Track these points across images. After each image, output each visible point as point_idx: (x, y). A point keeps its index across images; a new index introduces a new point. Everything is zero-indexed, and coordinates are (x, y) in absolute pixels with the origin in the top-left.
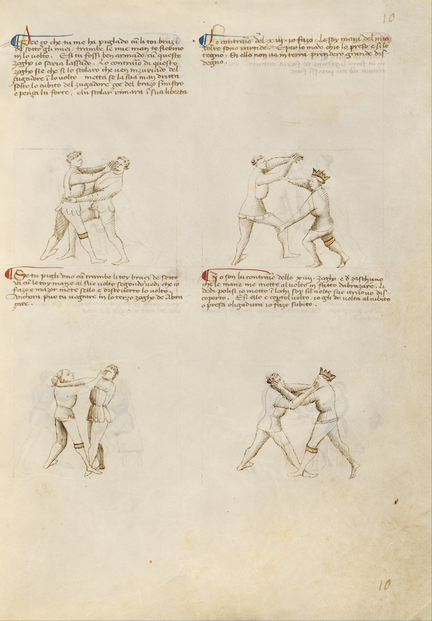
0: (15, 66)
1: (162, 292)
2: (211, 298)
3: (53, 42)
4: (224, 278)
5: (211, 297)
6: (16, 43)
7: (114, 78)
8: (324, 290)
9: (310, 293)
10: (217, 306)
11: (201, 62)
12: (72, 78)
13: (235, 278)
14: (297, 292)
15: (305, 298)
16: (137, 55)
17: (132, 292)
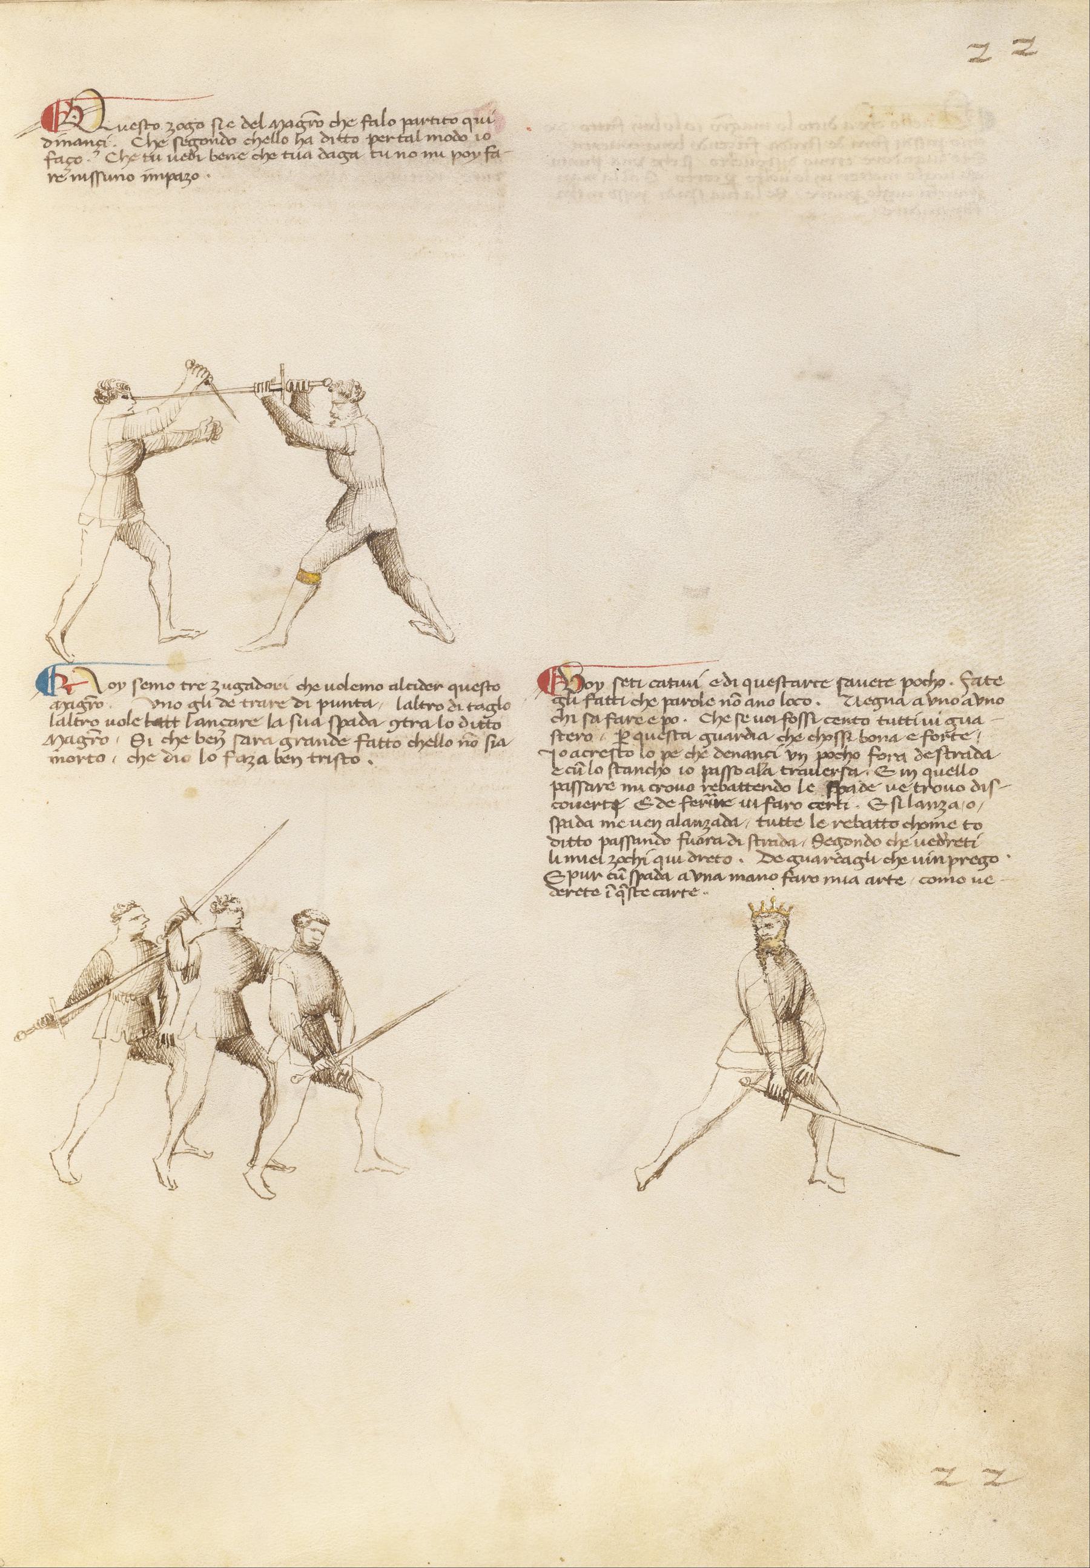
0: (614, 865)
6: (50, 685)
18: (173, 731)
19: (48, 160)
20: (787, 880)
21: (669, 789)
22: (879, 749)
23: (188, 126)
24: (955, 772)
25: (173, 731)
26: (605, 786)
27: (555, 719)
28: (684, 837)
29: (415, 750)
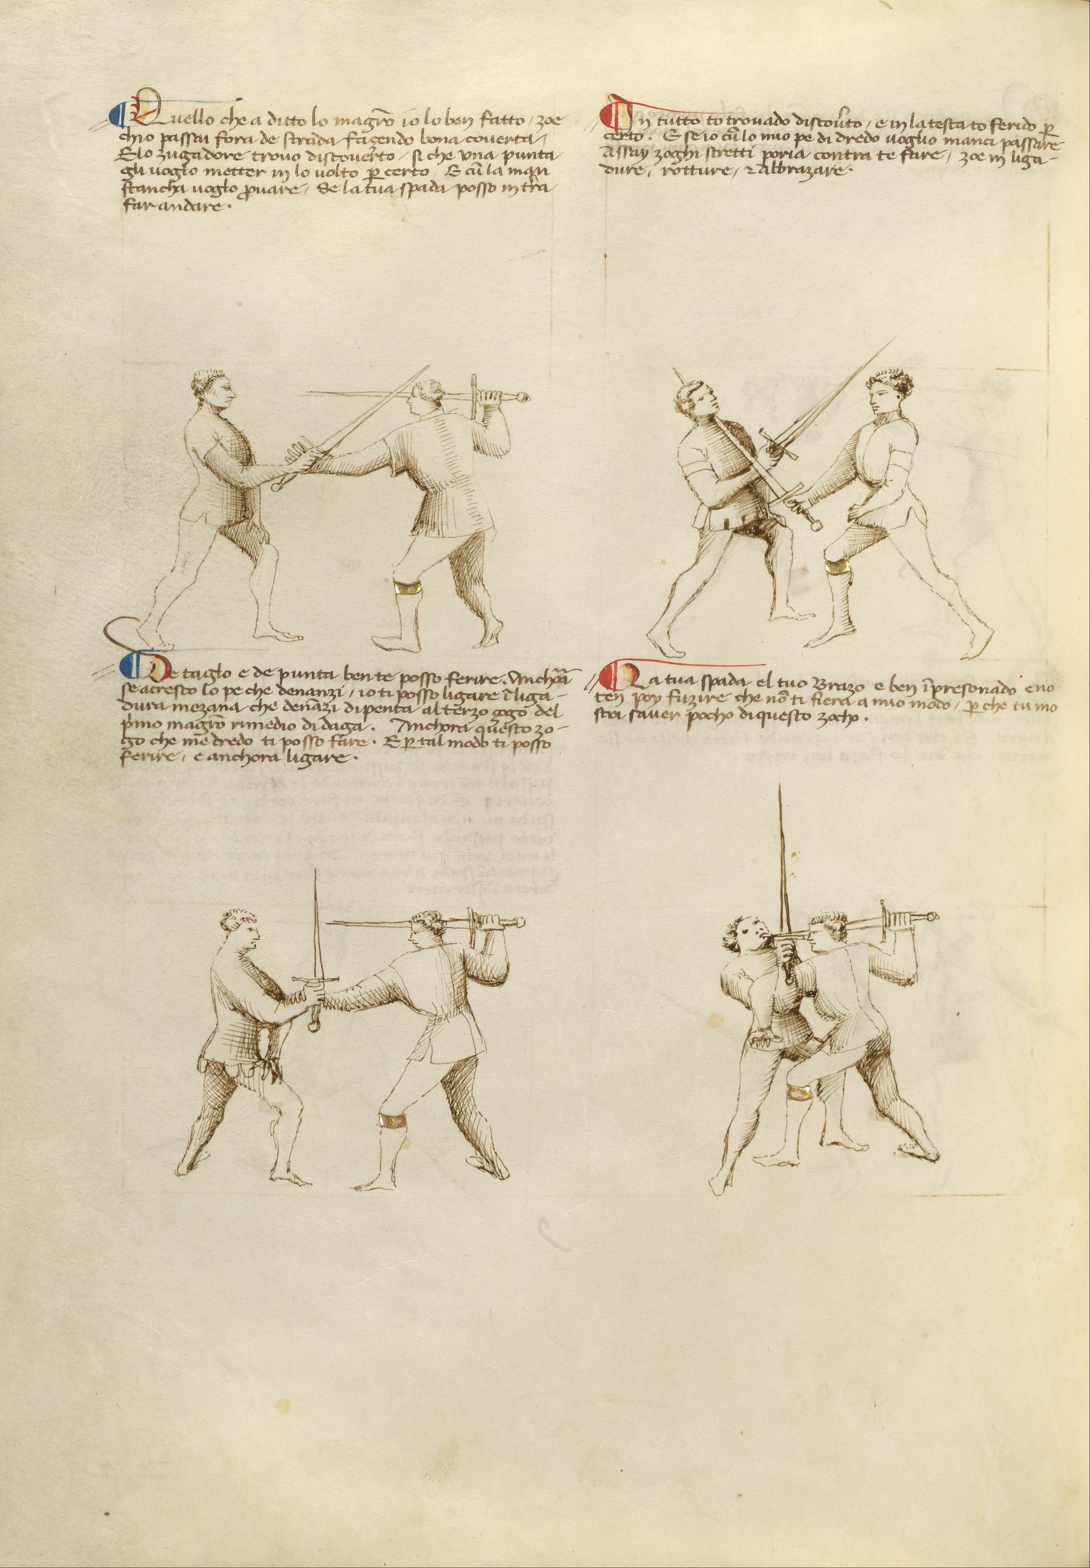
2: (370, 710)
3: (542, 678)
5: (770, 152)
7: (698, 137)
8: (325, 164)
10: (170, 693)
14: (437, 680)
16: (729, 679)
18: (921, 131)
21: (275, 157)
22: (679, 692)
23: (675, 155)
24: (193, 120)
25: (921, 131)
27: (154, 741)
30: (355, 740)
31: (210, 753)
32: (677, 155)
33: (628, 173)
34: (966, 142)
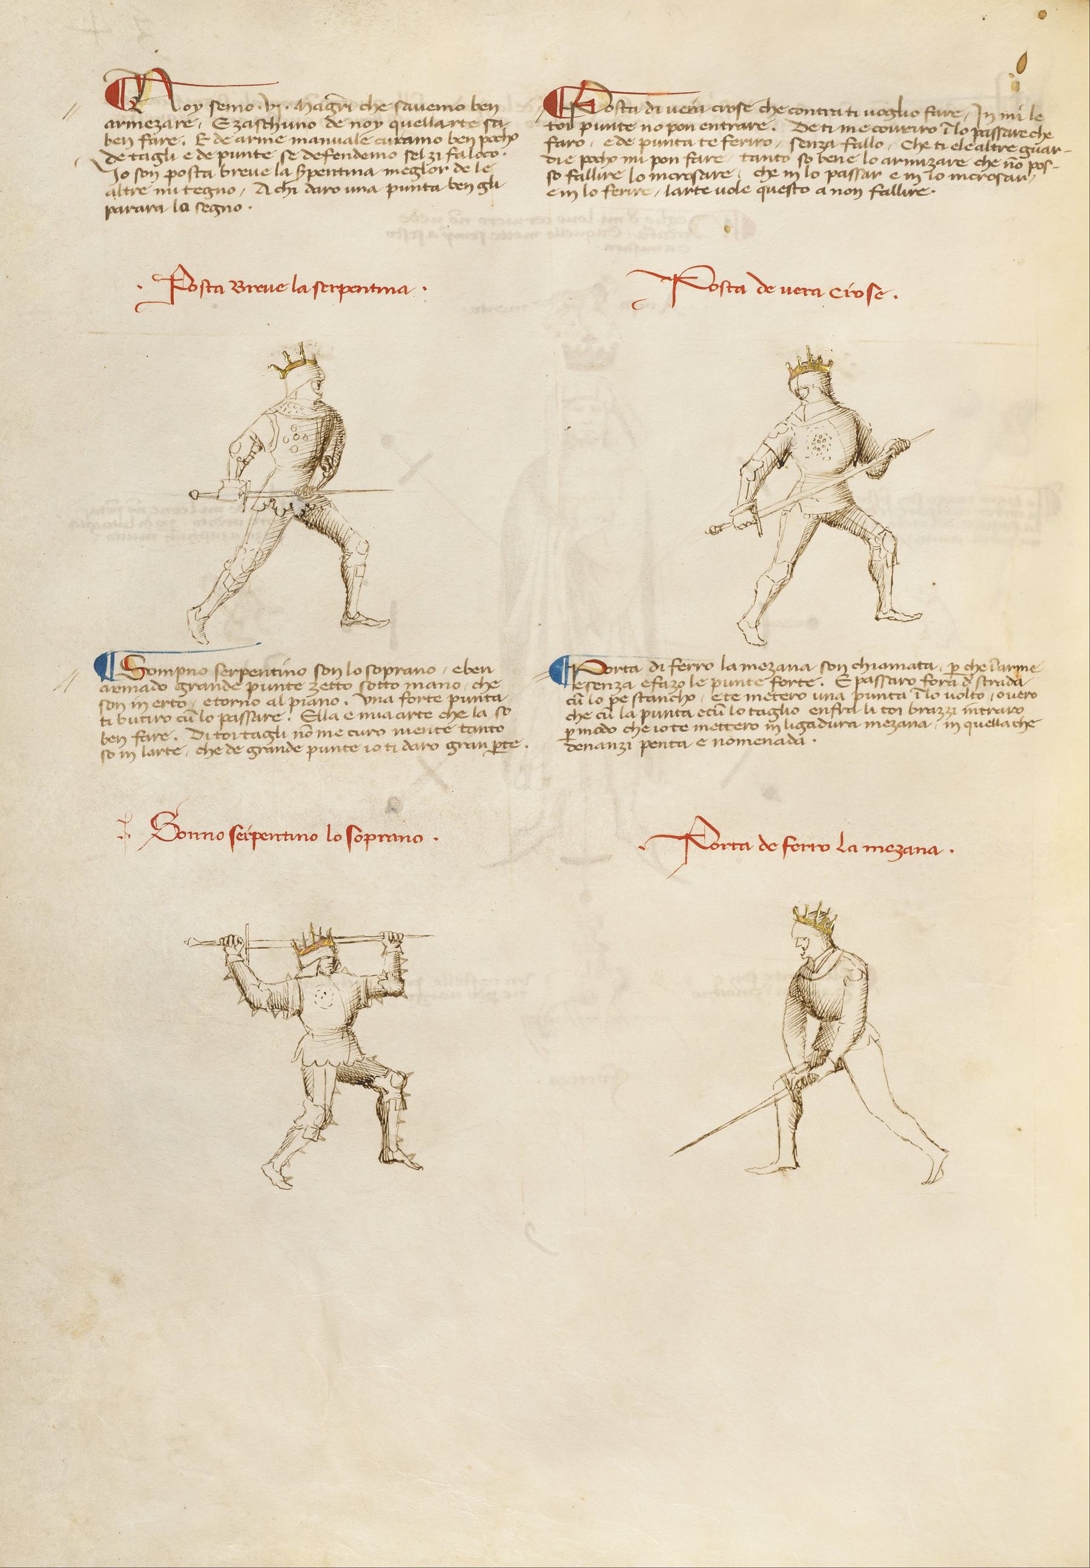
1: (777, 161)
4: (922, 115)
9: (226, 194)
11: (644, 754)
12: (495, 730)
13: (576, 197)
15: (895, 697)
17: (746, 144)
19: (549, 143)
20: (876, 195)
26: (720, 175)
28: (675, 664)
29: (281, 194)
30: (749, 724)
31: (882, 149)
32: (332, 107)
33: (324, 193)
34: (379, 124)
